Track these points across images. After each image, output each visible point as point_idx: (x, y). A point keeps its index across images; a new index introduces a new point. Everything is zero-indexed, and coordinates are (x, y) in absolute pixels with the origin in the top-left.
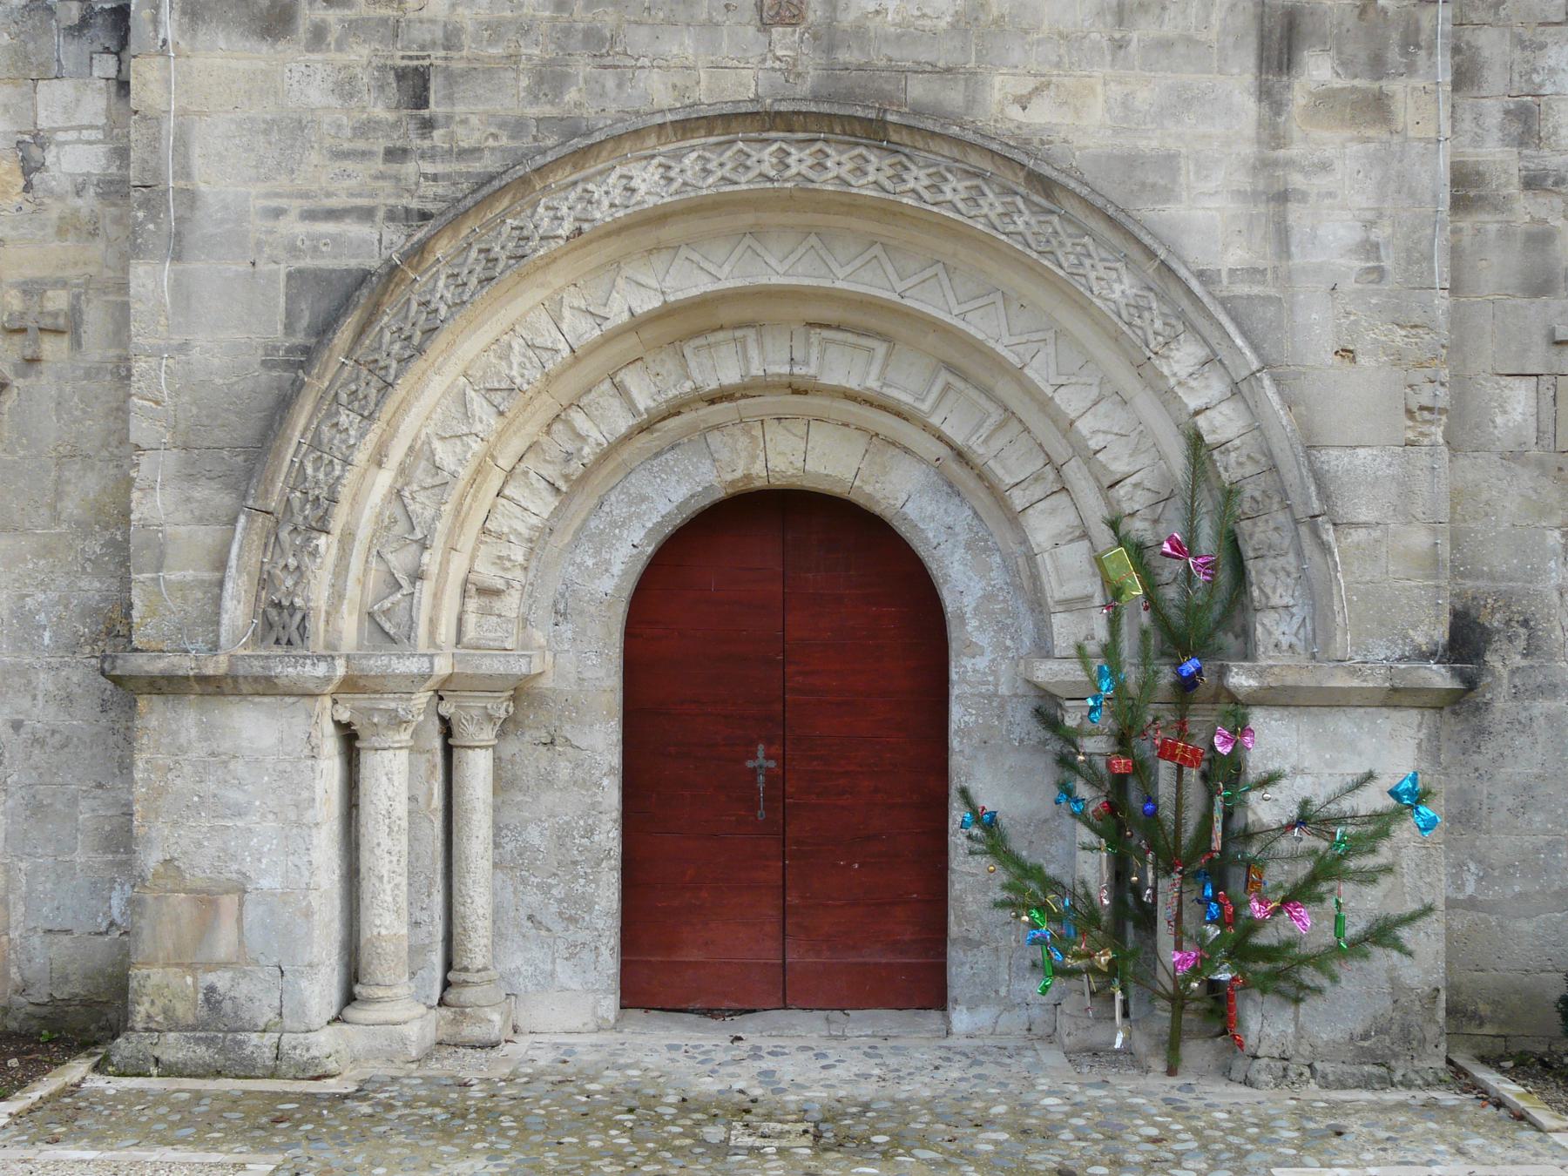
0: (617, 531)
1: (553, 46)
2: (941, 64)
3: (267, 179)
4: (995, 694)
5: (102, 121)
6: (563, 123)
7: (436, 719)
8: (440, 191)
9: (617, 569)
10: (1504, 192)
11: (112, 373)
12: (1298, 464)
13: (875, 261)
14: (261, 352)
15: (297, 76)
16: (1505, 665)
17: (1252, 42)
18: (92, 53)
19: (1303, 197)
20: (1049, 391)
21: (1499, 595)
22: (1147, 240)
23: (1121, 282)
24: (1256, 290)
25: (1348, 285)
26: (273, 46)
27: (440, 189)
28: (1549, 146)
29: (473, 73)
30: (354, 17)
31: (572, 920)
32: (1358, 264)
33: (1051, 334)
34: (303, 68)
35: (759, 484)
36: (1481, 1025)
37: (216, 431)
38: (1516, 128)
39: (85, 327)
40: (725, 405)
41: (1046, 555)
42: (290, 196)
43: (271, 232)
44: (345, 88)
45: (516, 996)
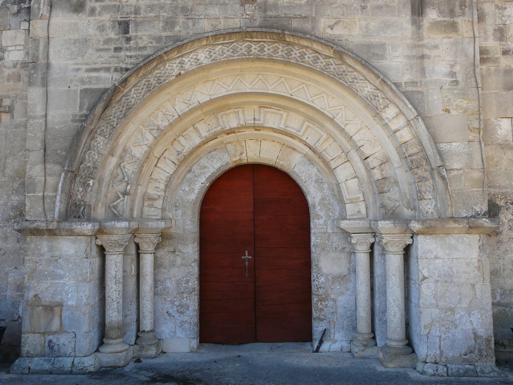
0: (196, 178)
1: (171, 13)
2: (303, 15)
3: (74, 59)
4: (327, 232)
5: (23, 43)
6: (174, 38)
7: (134, 243)
8: (132, 61)
9: (196, 191)
10: (496, 56)
11: (24, 126)
12: (432, 148)
13: (282, 83)
14: (71, 117)
15: (85, 25)
16: (506, 218)
17: (409, 6)
18: (20, 21)
19: (429, 57)
20: (343, 126)
21: (503, 194)
22: (376, 72)
23: (367, 88)
24: (414, 89)
25: (446, 86)
26: (77, 15)
27: (133, 60)
28: (510, 41)
29: (144, 22)
30: (105, 5)
31: (182, 313)
32: (449, 79)
33: (343, 107)
34: (87, 22)
35: (244, 162)
36: (505, 348)
37: (56, 144)
38: (499, 35)
39: (15, 111)
40: (232, 135)
41: (343, 184)
42: (82, 64)
43: (75, 76)
44: (101, 28)
45: (162, 340)
